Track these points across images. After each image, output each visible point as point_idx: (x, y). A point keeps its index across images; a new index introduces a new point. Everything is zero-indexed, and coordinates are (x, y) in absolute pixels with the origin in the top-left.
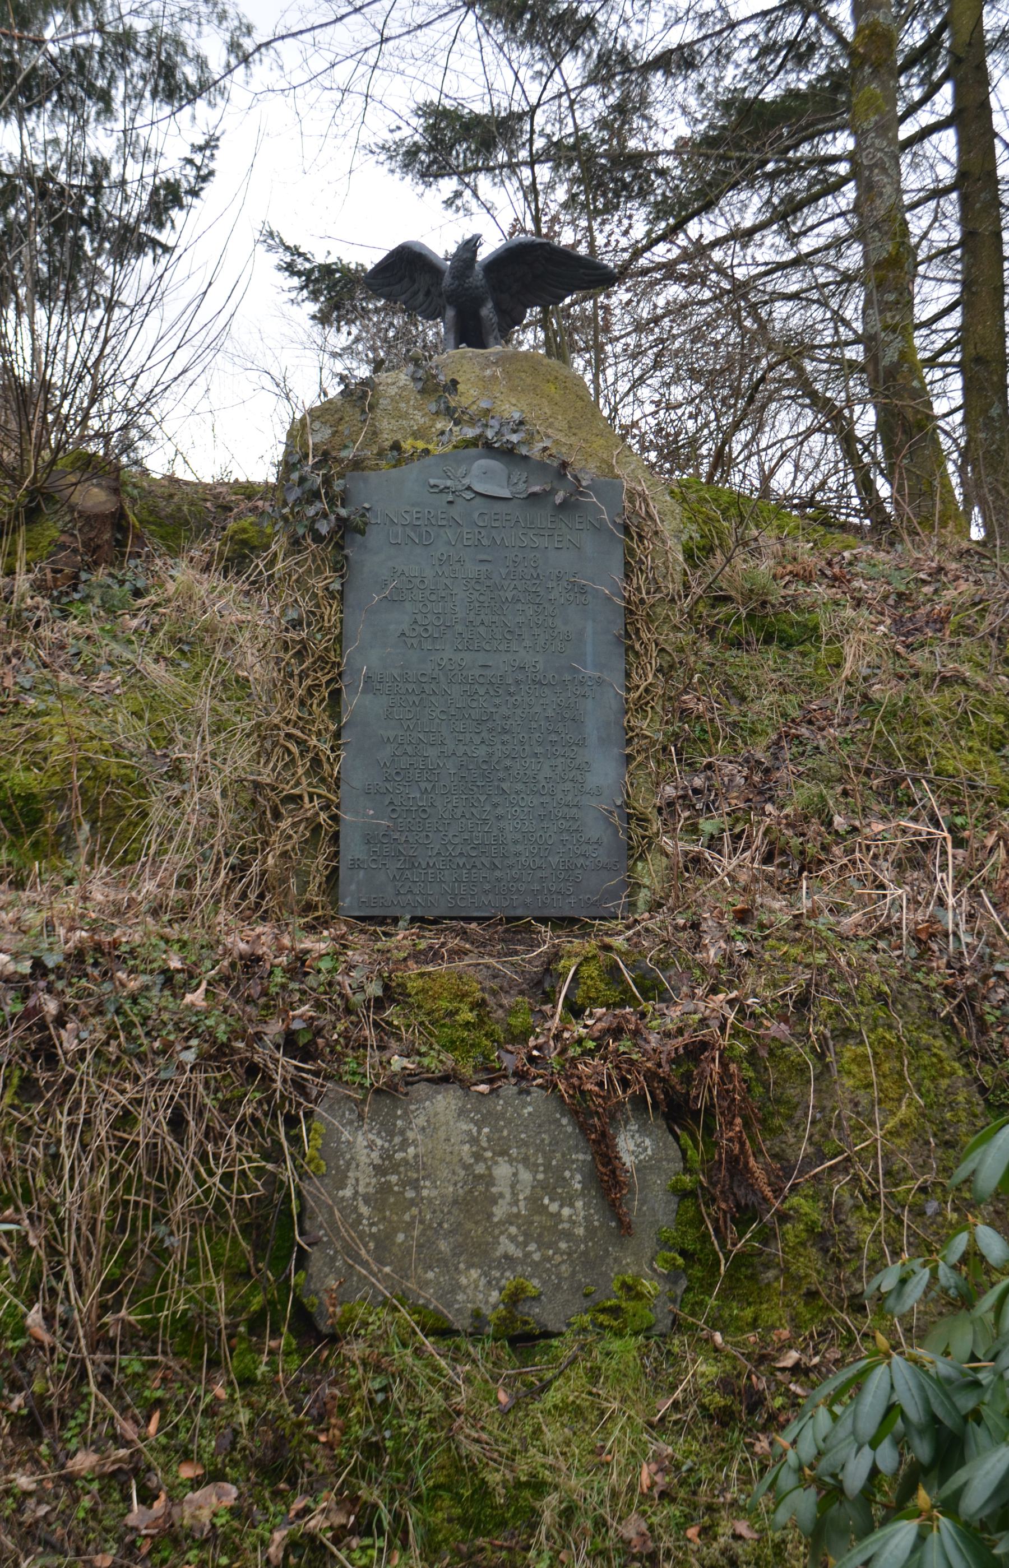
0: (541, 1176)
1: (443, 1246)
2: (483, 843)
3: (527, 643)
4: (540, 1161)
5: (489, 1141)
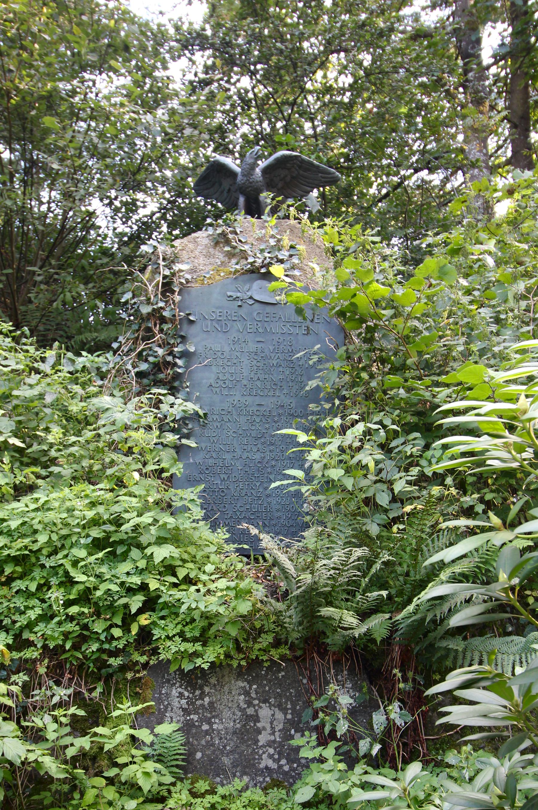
0: (289, 716)
1: (226, 760)
2: (258, 511)
3: (285, 391)
4: (289, 706)
5: (257, 693)
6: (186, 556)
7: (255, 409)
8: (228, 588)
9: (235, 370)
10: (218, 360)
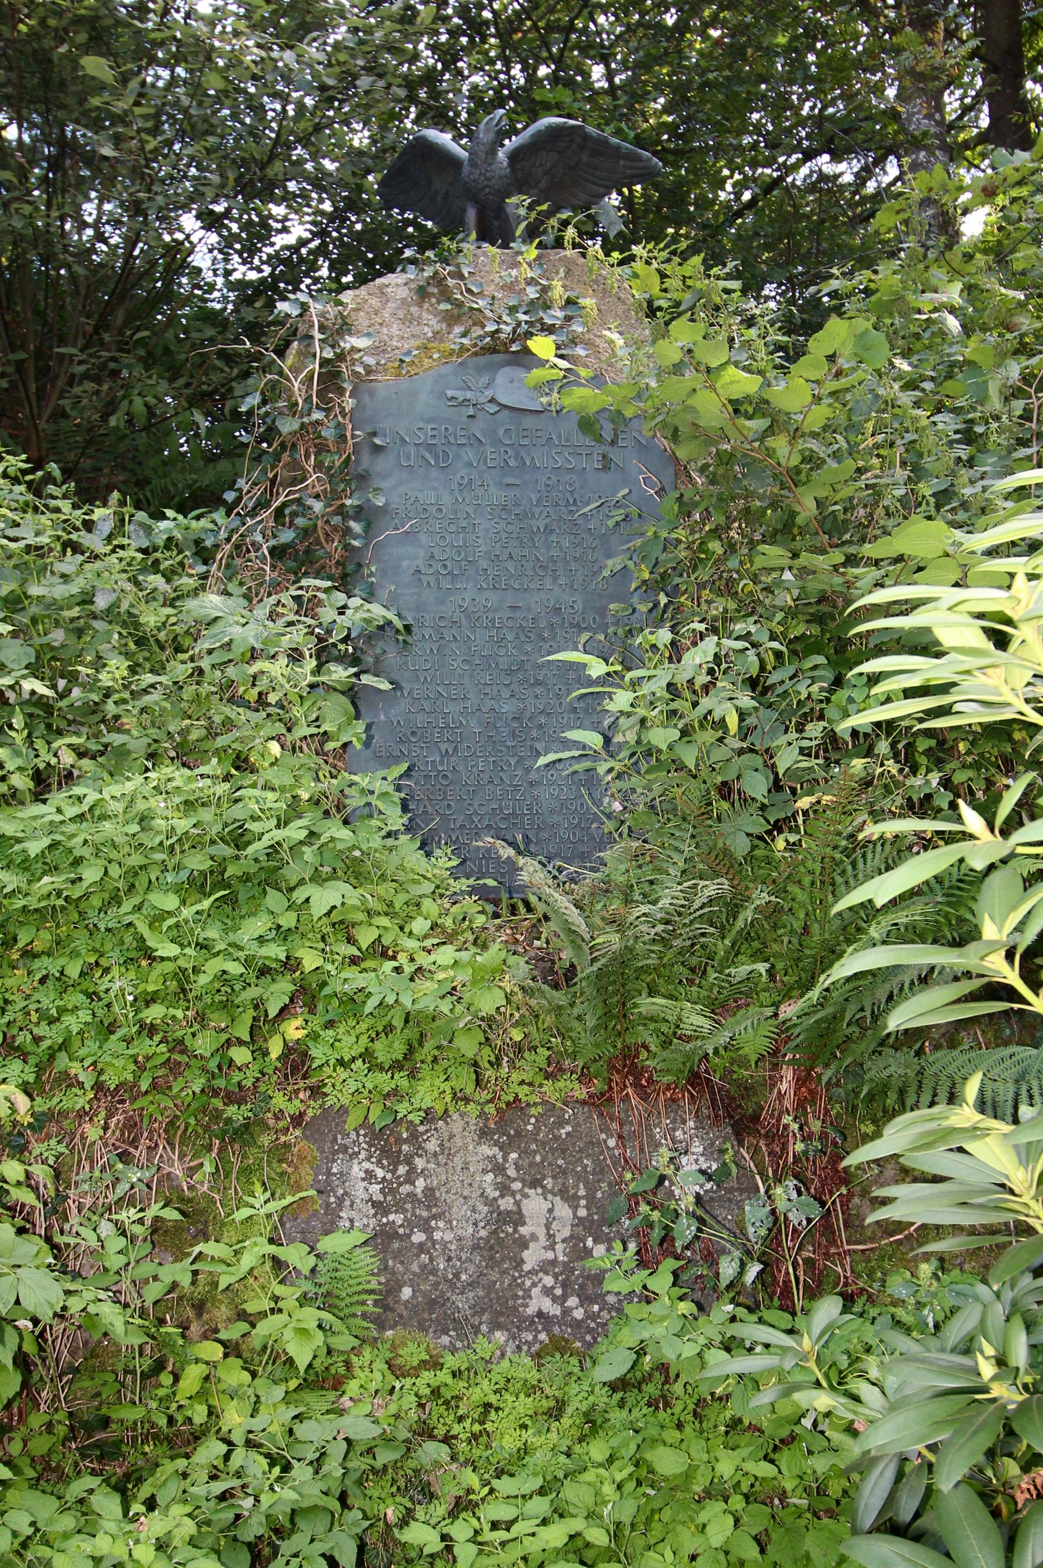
6: (373, 903)
7: (505, 614)
9: (465, 541)
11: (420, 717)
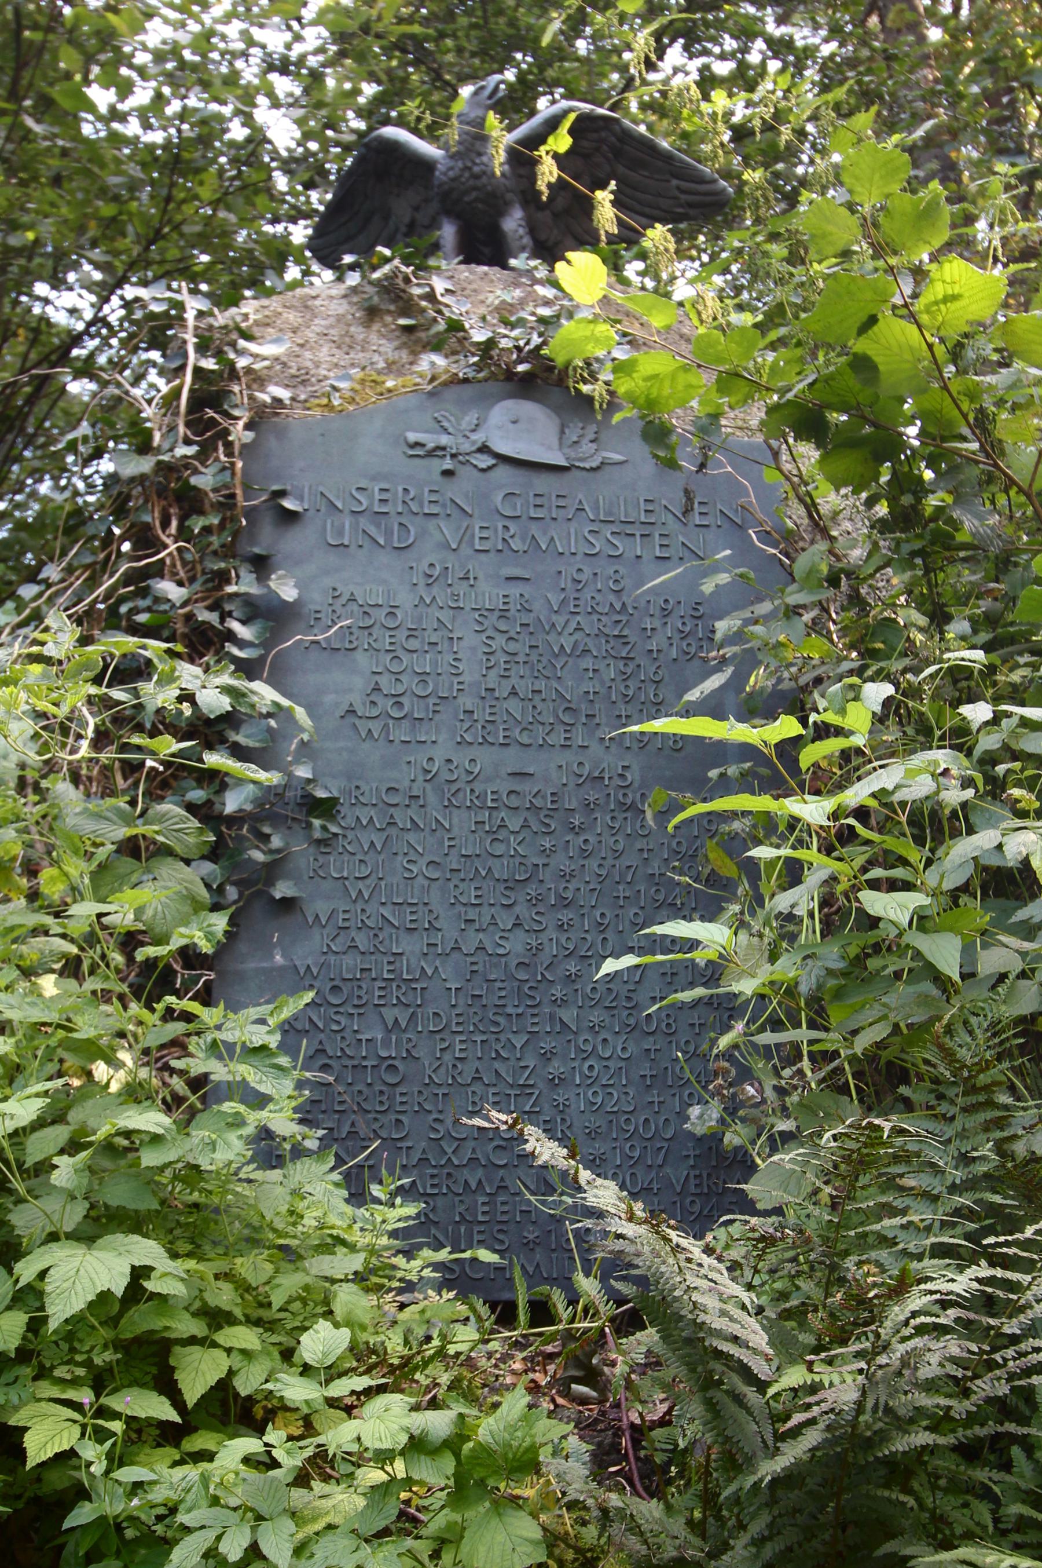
6: (224, 1296)
7: (504, 786)
8: (417, 1445)
9: (435, 663)
10: (376, 632)
11: (348, 960)
